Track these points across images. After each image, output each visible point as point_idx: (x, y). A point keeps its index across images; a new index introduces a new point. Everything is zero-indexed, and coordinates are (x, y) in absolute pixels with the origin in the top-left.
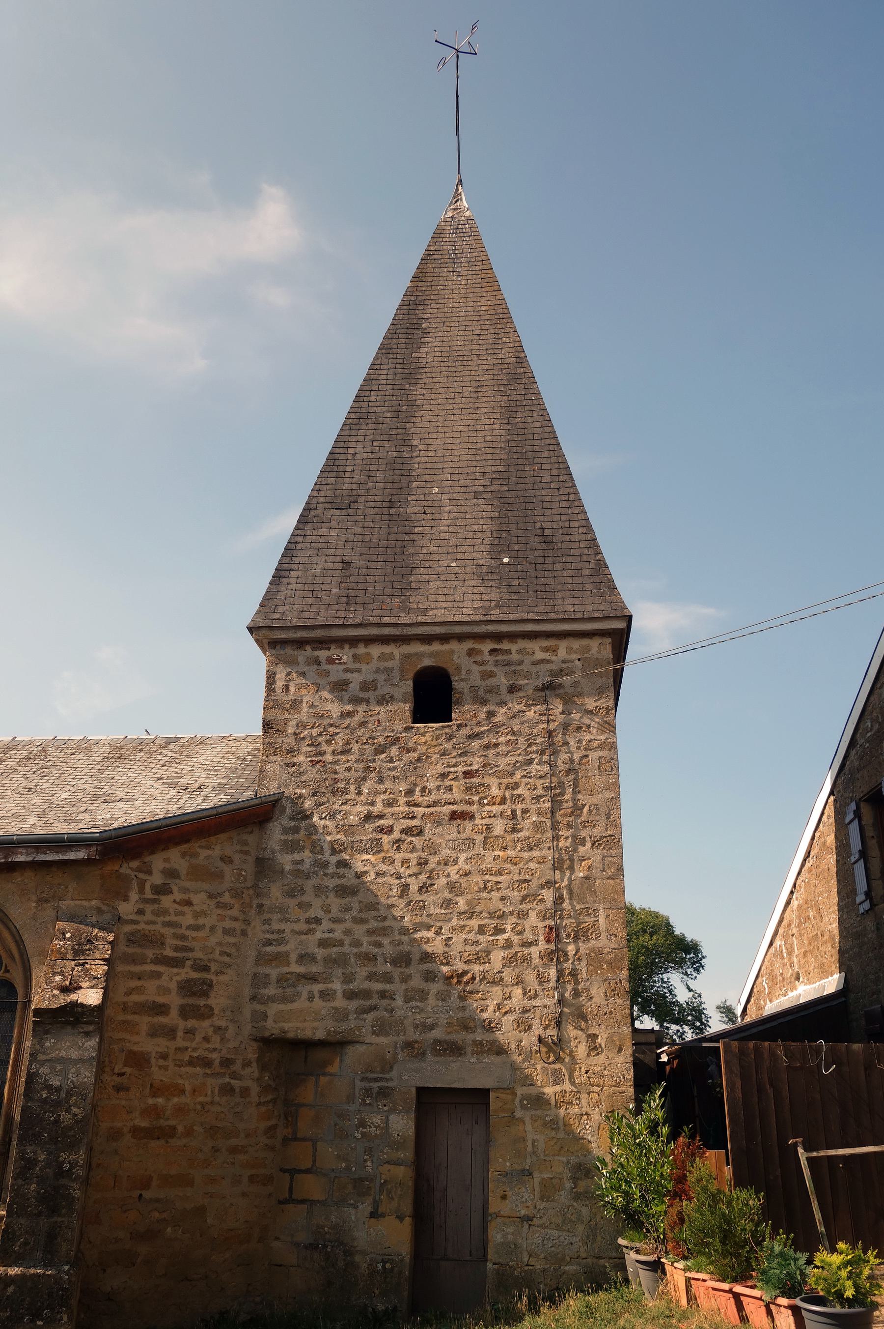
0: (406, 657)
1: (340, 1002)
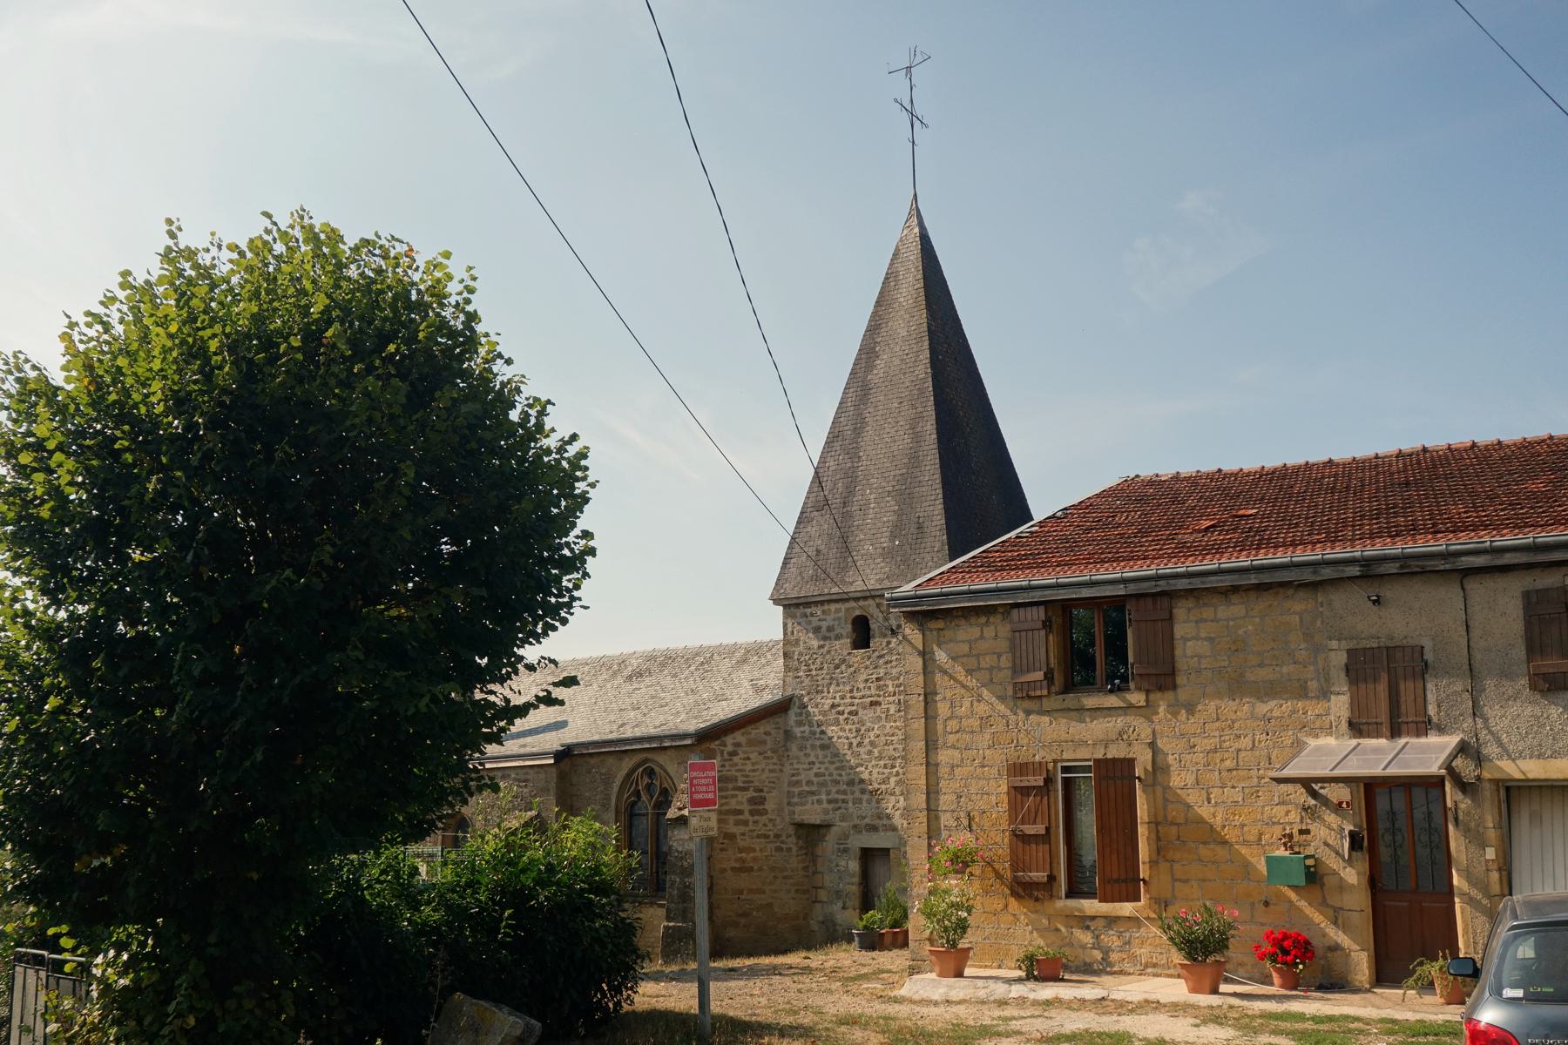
0: (847, 610)
1: (825, 805)
